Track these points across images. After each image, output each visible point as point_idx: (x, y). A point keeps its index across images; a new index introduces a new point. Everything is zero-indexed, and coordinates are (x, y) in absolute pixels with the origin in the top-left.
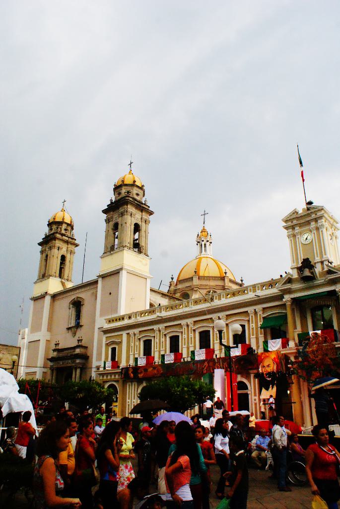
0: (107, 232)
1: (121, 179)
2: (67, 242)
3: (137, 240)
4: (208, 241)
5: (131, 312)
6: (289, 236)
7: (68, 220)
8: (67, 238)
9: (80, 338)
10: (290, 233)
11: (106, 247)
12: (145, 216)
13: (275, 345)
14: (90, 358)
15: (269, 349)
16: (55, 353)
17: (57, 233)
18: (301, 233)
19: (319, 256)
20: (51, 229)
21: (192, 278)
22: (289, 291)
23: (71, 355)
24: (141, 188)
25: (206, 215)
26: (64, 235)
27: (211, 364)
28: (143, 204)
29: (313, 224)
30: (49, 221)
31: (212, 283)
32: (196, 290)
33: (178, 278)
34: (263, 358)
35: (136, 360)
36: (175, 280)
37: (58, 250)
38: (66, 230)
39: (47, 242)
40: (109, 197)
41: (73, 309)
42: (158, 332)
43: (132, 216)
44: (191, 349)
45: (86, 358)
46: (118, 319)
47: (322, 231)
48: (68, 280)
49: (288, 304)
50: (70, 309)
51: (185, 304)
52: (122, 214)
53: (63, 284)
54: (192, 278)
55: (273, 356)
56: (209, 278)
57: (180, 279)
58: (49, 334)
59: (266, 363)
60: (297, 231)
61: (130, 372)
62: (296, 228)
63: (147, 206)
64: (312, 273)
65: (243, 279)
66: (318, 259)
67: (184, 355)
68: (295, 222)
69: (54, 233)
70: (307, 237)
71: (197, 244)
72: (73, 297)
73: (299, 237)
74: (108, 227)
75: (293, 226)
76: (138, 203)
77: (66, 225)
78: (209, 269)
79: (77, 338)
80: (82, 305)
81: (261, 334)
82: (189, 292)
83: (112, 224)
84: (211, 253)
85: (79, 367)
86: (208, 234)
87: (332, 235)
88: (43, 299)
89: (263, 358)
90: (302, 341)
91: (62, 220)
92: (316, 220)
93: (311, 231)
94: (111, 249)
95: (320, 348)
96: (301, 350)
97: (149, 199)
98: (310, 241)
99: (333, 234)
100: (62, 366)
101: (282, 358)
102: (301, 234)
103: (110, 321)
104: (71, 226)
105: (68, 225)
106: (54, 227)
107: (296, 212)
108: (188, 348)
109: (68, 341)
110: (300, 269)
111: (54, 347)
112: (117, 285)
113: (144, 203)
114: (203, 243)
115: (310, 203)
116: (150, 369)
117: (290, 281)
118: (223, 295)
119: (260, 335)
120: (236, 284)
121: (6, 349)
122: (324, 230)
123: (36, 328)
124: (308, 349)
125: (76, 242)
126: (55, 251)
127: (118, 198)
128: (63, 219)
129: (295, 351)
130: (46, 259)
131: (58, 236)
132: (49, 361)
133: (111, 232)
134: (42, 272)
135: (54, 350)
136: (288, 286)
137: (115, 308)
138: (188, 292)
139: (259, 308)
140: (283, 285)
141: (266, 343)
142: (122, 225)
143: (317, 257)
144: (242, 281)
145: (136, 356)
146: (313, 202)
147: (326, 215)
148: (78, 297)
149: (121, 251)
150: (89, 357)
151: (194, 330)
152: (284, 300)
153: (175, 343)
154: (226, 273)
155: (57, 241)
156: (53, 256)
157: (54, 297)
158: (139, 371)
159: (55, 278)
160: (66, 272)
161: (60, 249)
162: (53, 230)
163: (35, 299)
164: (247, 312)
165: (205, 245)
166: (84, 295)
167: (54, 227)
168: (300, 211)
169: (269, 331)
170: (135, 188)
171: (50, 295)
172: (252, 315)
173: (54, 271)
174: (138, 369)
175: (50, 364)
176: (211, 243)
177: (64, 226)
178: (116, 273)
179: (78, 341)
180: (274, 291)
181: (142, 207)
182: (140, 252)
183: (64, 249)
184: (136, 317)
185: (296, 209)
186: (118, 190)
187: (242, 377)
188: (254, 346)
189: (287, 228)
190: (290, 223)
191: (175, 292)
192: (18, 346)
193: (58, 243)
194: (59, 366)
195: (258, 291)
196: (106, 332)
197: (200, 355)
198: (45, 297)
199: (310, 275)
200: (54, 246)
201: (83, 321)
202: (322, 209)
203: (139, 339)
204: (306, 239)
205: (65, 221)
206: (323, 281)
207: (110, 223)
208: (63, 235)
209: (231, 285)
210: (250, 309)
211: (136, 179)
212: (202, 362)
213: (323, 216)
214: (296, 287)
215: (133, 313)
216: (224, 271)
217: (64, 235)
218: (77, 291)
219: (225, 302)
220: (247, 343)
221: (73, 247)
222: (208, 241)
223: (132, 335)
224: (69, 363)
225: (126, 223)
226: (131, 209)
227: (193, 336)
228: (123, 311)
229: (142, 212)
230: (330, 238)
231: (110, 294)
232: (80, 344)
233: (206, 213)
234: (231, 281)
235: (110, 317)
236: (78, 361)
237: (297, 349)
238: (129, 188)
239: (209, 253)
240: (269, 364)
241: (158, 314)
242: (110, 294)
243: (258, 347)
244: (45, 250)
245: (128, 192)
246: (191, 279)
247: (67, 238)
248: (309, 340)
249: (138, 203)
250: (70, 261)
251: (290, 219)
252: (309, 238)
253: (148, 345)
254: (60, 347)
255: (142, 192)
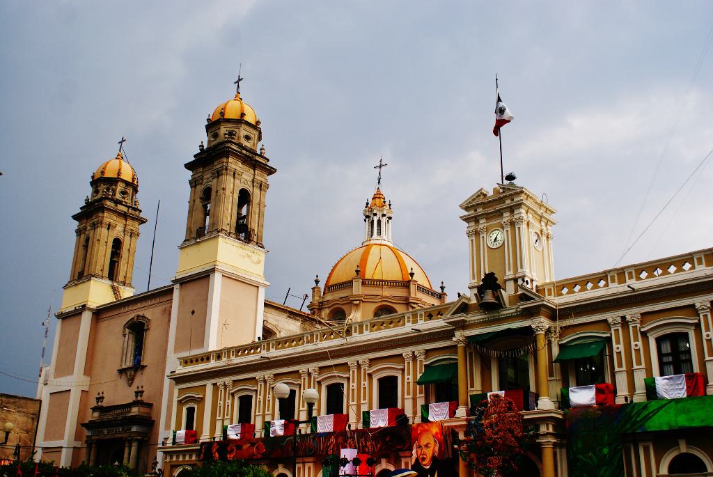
0: (192, 202)
1: (222, 106)
2: (124, 216)
3: (244, 217)
4: (384, 215)
5: (223, 347)
6: (469, 234)
7: (127, 175)
8: (125, 209)
9: (140, 389)
10: (471, 229)
11: (189, 230)
12: (260, 176)
13: (439, 413)
14: (156, 422)
15: (430, 418)
16: (96, 414)
17: (107, 198)
18: (487, 230)
19: (512, 269)
20: (96, 192)
21: (351, 282)
22: (463, 325)
23: (124, 418)
24: (255, 126)
25: (383, 168)
26: (120, 202)
27: (340, 440)
28: (257, 155)
29: (506, 216)
30: (93, 177)
31: (387, 292)
32: (357, 305)
33: (327, 282)
34: (419, 432)
35: (225, 430)
36: (322, 285)
37: (108, 229)
38: (123, 193)
39: (89, 214)
40: (199, 139)
41: (131, 336)
42: (263, 384)
43: (236, 178)
44: (364, 408)
45: (148, 423)
46: (194, 360)
47: (519, 228)
48: (124, 284)
49: (461, 345)
50: (125, 336)
51: (307, 337)
52: (218, 172)
53: (115, 290)
54: (351, 282)
55: (435, 430)
56: (380, 283)
57: (331, 283)
58: (88, 379)
59: (424, 441)
60: (481, 226)
61: (215, 450)
62: (481, 221)
63: (265, 158)
64: (498, 298)
65: (444, 285)
66: (510, 274)
67: (352, 419)
68: (480, 210)
69: (101, 199)
70: (498, 236)
71: (365, 221)
72: (132, 316)
73: (485, 235)
74: (193, 193)
75: (475, 217)
76: (248, 154)
77: (123, 185)
78: (382, 266)
79: (134, 388)
80: (147, 330)
81: (421, 393)
82: (345, 308)
83: (200, 188)
84: (390, 238)
85: (136, 440)
86: (384, 202)
87: (539, 235)
88: (75, 320)
89: (419, 432)
90: (476, 407)
91: (116, 176)
92: (511, 209)
93: (503, 228)
94: (198, 233)
95: (501, 419)
96: (473, 422)
97: (270, 147)
98: (501, 243)
99: (541, 231)
100: (108, 437)
101: (448, 433)
102: (487, 231)
103: (186, 362)
104: (133, 186)
105: (127, 183)
106: (102, 187)
107: (481, 193)
108: (359, 406)
109: (119, 394)
110: (481, 290)
111: (93, 403)
112: (205, 299)
113: (259, 152)
114: (376, 219)
115: (511, 178)
116: (246, 447)
117: (464, 308)
118: (367, 326)
119: (418, 395)
120: (433, 294)
121: (14, 403)
122: (523, 226)
123: (64, 368)
124: (485, 422)
125: (142, 215)
126: (103, 231)
127: (213, 143)
128: (119, 174)
129: (465, 423)
130: (85, 244)
131: (109, 204)
132: (84, 428)
133: (199, 203)
134: (79, 269)
135: (95, 409)
136: (462, 317)
137: (201, 338)
138: (343, 307)
139: (419, 349)
140: (453, 314)
141: (426, 408)
142: (217, 192)
143: (509, 270)
144: (442, 288)
145: (268, 419)
146: (516, 176)
147: (528, 203)
148: (138, 316)
149: (214, 238)
150: (154, 421)
151: (370, 375)
152: (454, 339)
153: (287, 406)
154: (412, 274)
155: (106, 214)
156: (99, 240)
157: (100, 314)
158: (229, 449)
159: (101, 280)
160: (122, 269)
161: (111, 228)
162: (101, 192)
163: (64, 317)
164: (401, 355)
165: (379, 222)
166: (151, 313)
167: (102, 187)
168: (490, 193)
169: (432, 388)
170: (243, 126)
171: (90, 309)
172: (409, 361)
173: (99, 267)
174: (228, 445)
175: (87, 433)
176: (390, 218)
177: (120, 187)
178: (204, 277)
179: (137, 393)
180: (438, 324)
181: (255, 161)
182: (248, 239)
183: (120, 228)
184: (229, 357)
185: (481, 189)
186: (214, 129)
187: (389, 462)
188: (408, 413)
189: (467, 219)
190: (473, 212)
191: (321, 306)
192: (38, 398)
193: (108, 218)
194: (102, 437)
195: (420, 322)
196: (179, 380)
197: (326, 424)
198: (81, 313)
199: (493, 301)
200: (101, 223)
201: (147, 359)
202: (522, 192)
203: (233, 395)
204: (495, 240)
205: (123, 177)
206: (514, 311)
207: (198, 187)
208: (117, 202)
209: (420, 295)
210: (406, 351)
211: (247, 110)
212: (327, 435)
213: (522, 204)
214: (472, 319)
215: (225, 349)
216: (410, 271)
217: (120, 202)
218: (139, 305)
219: (369, 338)
220: (399, 406)
221: (136, 224)
222: (384, 215)
223: (222, 388)
224: (119, 432)
225: (224, 189)
226: (234, 164)
227: (355, 387)
228: (213, 345)
229: (254, 170)
230: (536, 238)
231: (193, 312)
232: (139, 398)
233: (383, 163)
234: (421, 289)
235: (186, 354)
236: (134, 429)
237: (466, 420)
238: (231, 127)
239: (385, 237)
240: (428, 443)
241: (265, 353)
242: (193, 312)
243: (415, 413)
244: (85, 228)
245: (231, 134)
246: (348, 284)
247: (125, 209)
248: (486, 407)
249: (248, 154)
250: (129, 250)
251: (472, 206)
252: (499, 238)
253: (246, 404)
254: (105, 404)
255: (256, 133)
